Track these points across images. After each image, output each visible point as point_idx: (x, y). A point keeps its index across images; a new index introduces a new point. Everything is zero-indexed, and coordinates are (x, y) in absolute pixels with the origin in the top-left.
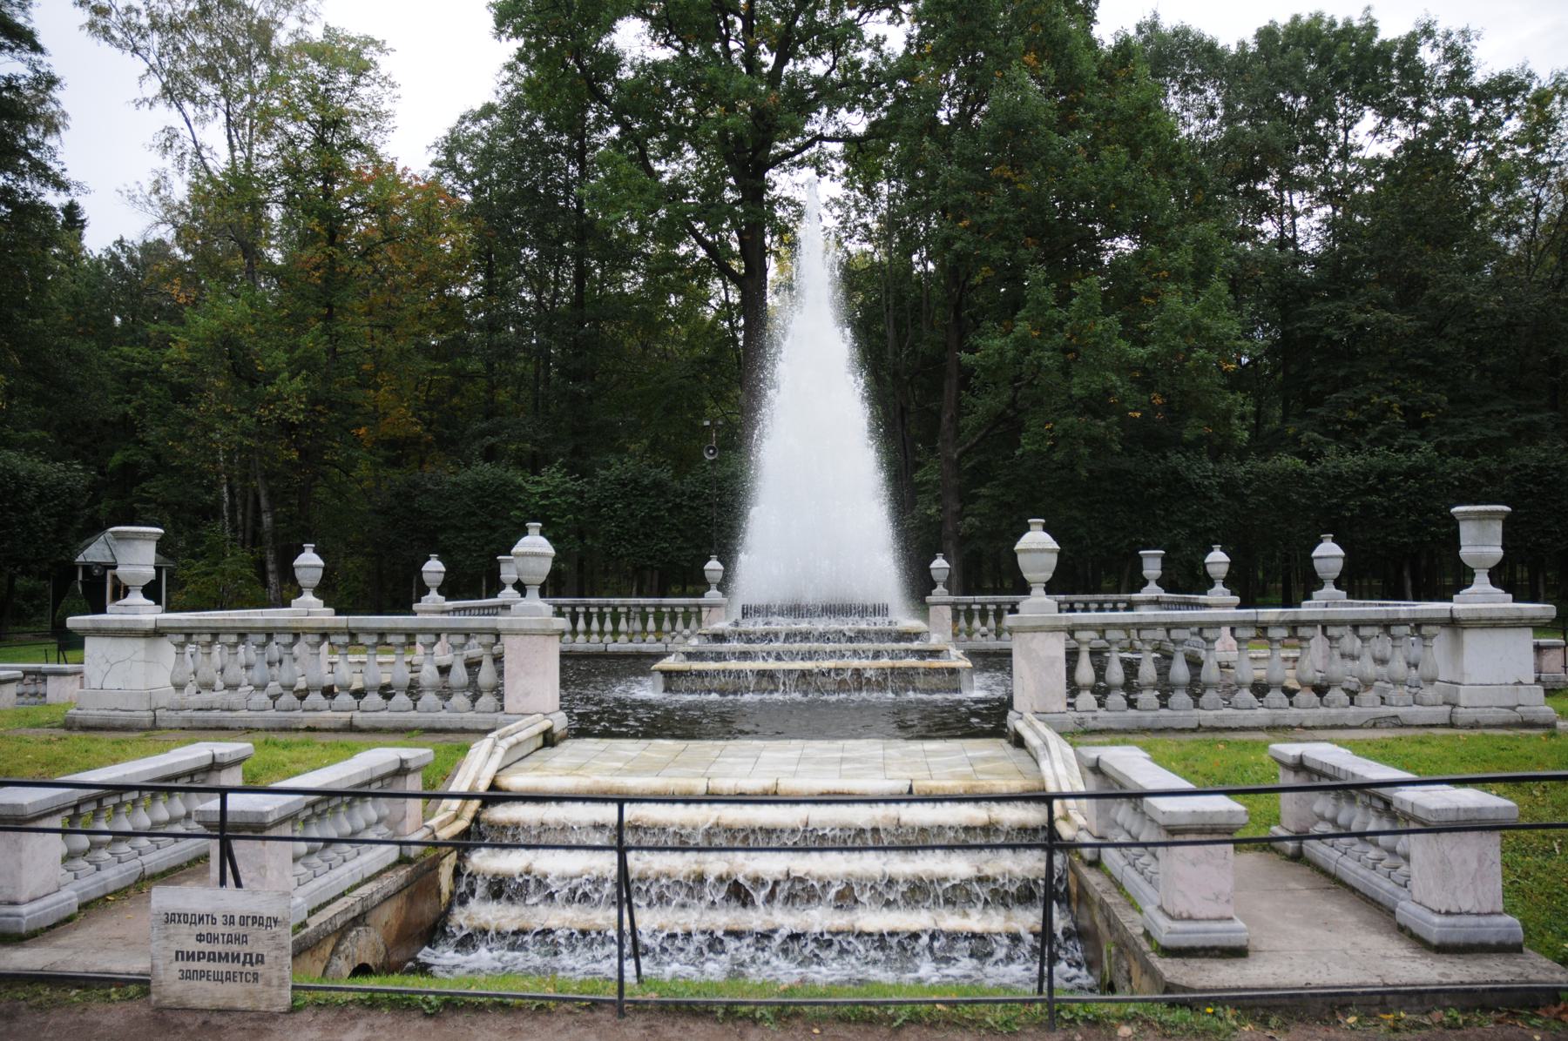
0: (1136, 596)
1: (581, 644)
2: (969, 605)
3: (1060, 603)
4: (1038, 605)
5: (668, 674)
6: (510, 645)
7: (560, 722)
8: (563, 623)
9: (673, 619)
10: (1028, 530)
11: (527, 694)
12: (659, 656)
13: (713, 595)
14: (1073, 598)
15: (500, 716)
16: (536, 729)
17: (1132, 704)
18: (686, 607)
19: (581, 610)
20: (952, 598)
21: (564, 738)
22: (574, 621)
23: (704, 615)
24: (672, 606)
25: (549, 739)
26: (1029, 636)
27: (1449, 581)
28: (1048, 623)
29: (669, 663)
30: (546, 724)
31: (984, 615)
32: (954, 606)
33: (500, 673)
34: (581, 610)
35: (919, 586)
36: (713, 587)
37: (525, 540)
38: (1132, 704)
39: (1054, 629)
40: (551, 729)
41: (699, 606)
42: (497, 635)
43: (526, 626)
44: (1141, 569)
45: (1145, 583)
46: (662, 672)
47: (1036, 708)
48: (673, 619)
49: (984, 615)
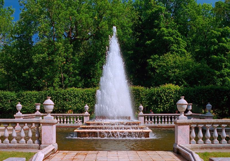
4: (182, 118)
7: (55, 146)
12: (76, 128)
13: (87, 113)
18: (161, 116)
35: (136, 109)
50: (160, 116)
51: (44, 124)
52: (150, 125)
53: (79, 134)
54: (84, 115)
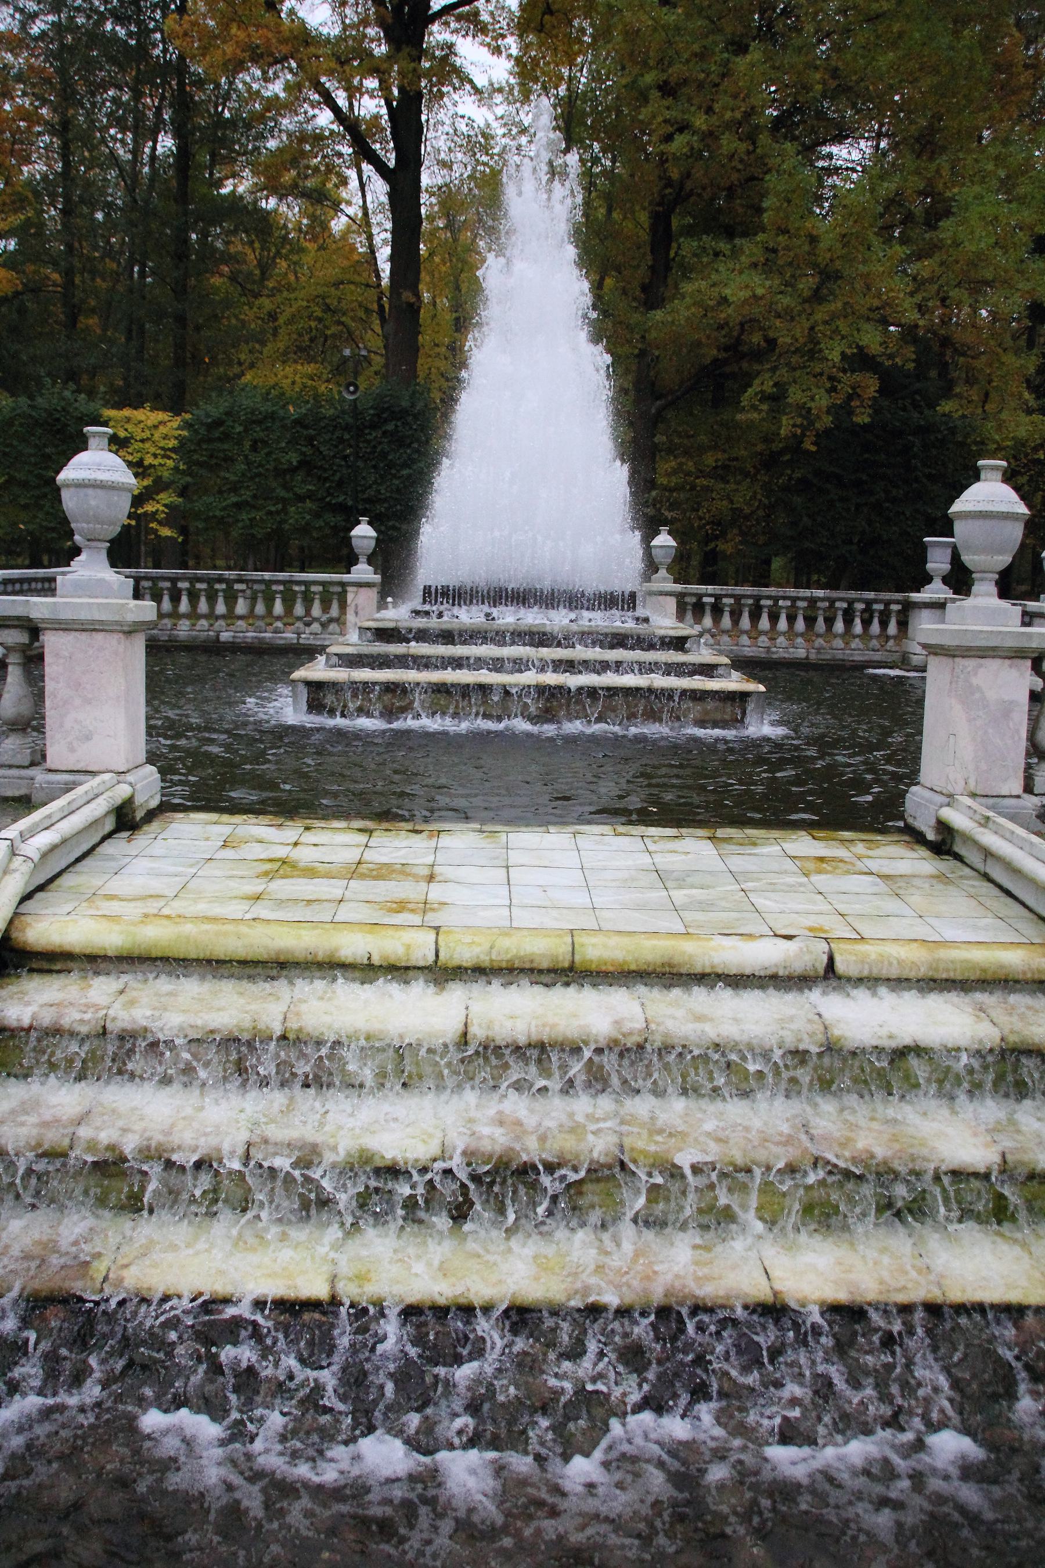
0: (915, 596)
1: (184, 629)
2: (700, 596)
3: (137, 580)
4: (92, 584)
5: (316, 687)
6: (52, 642)
7: (146, 785)
8: (146, 609)
9: (308, 601)
10: (978, 479)
11: (88, 738)
13: (363, 571)
14: (835, 594)
15: (39, 776)
16: (100, 807)
19: (183, 585)
20: (679, 587)
21: (151, 815)
22: (175, 599)
23: (350, 597)
24: (307, 584)
25: (126, 820)
26: (970, 663)
27: (1023, 588)
28: (1010, 643)
29: (318, 670)
30: (123, 791)
31: (717, 610)
32: (680, 597)
33: (39, 697)
34: (860, 606)
36: (363, 559)
37: (82, 457)
39: (1017, 654)
40: (129, 802)
41: (343, 584)
42: (34, 630)
43: (84, 615)
44: (925, 561)
45: (929, 579)
46: (309, 684)
47: (972, 786)
48: (308, 601)
49: (717, 610)
51: (65, 626)
52: (748, 648)
53: (318, 695)
54: (346, 577)
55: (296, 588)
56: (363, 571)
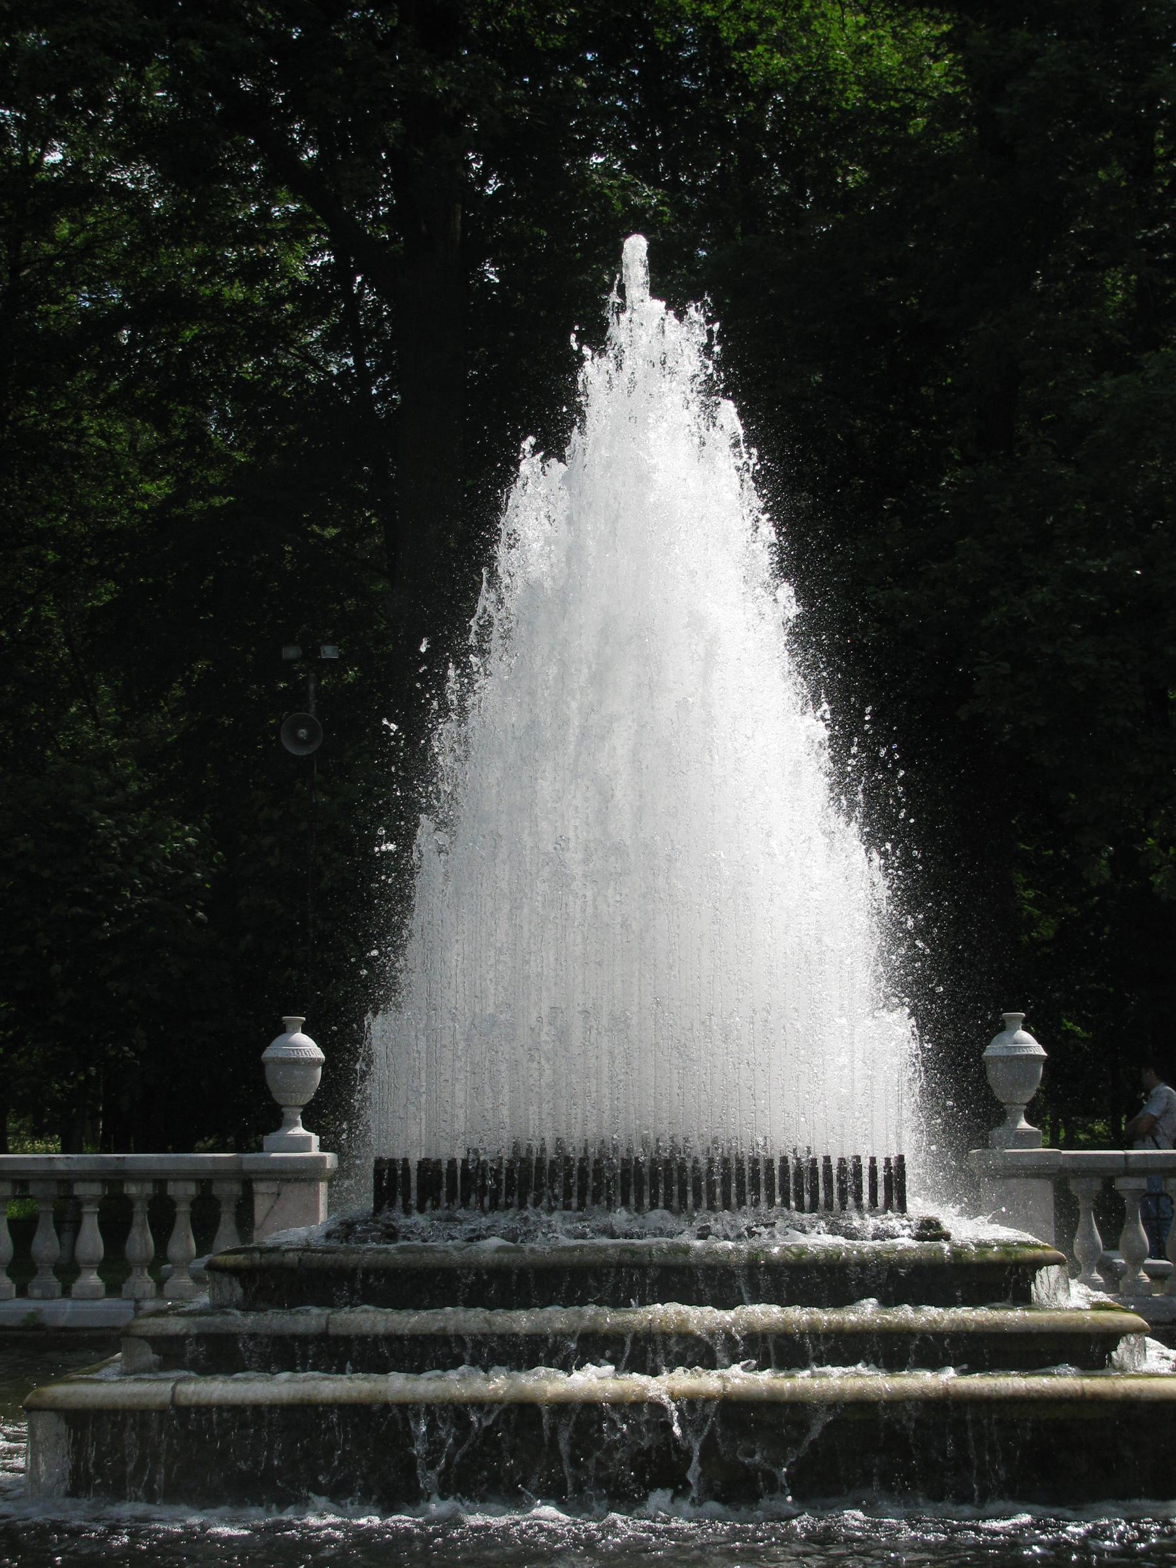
12: (91, 1345)
13: (302, 1141)
17: (113, 1289)
23: (261, 1206)
24: (160, 1181)
38: (113, 1289)
41: (247, 1181)
50: (87, 1177)
55: (132, 1189)
56: (302, 1141)
